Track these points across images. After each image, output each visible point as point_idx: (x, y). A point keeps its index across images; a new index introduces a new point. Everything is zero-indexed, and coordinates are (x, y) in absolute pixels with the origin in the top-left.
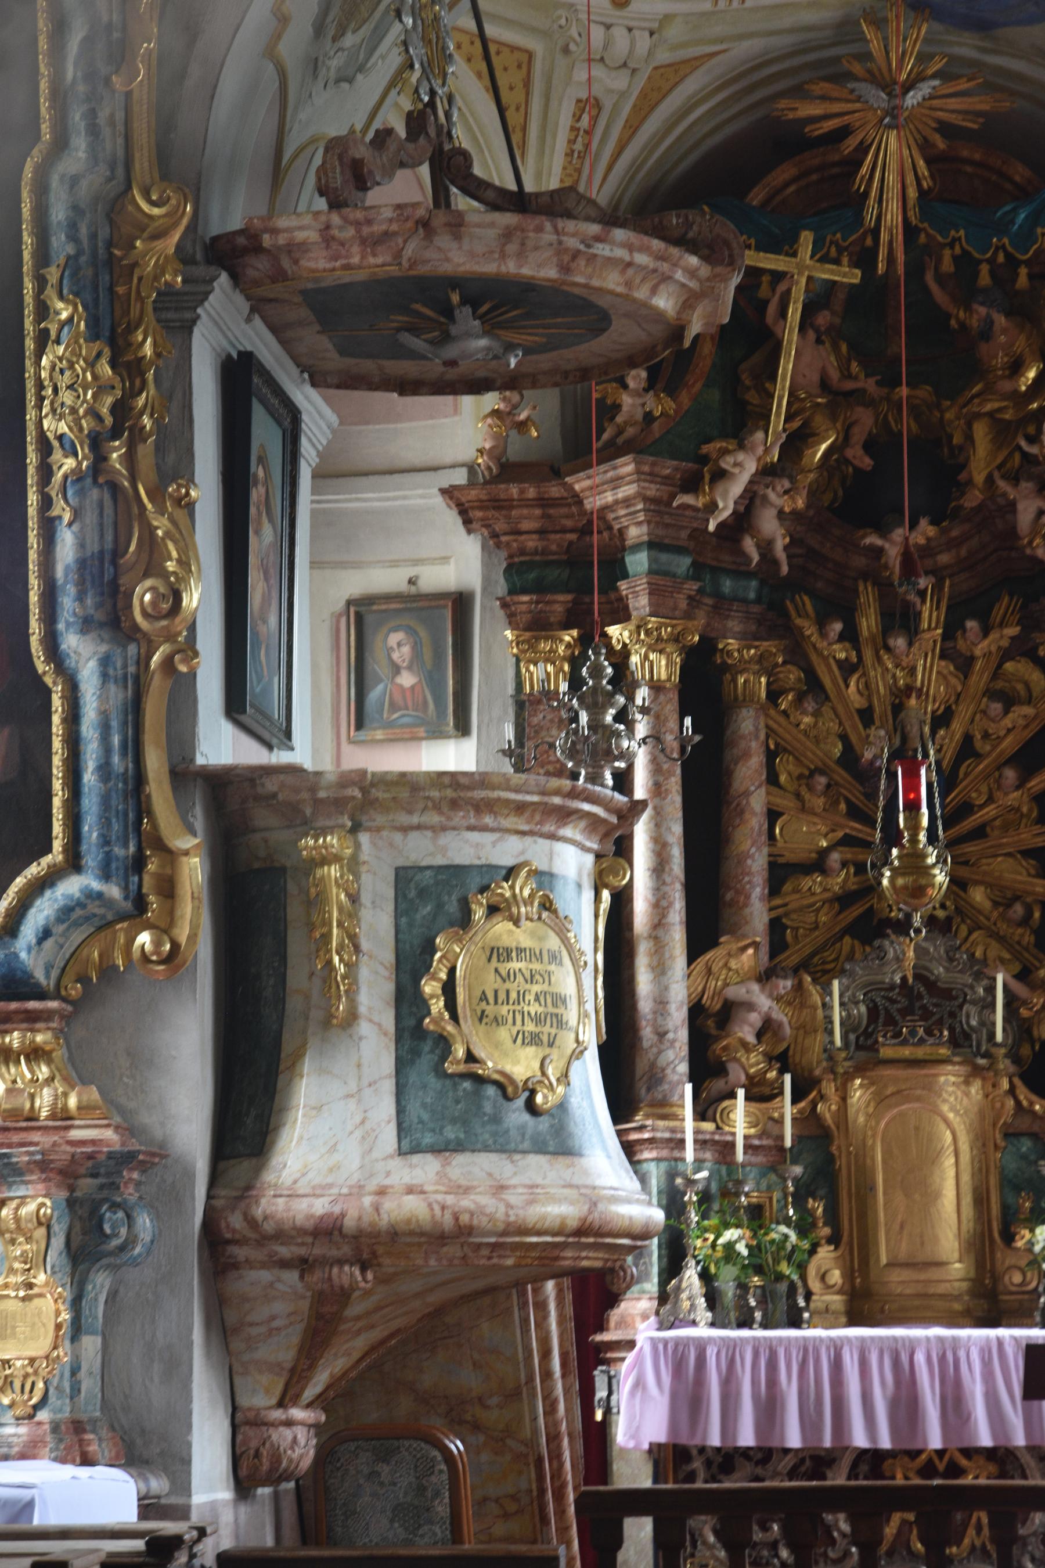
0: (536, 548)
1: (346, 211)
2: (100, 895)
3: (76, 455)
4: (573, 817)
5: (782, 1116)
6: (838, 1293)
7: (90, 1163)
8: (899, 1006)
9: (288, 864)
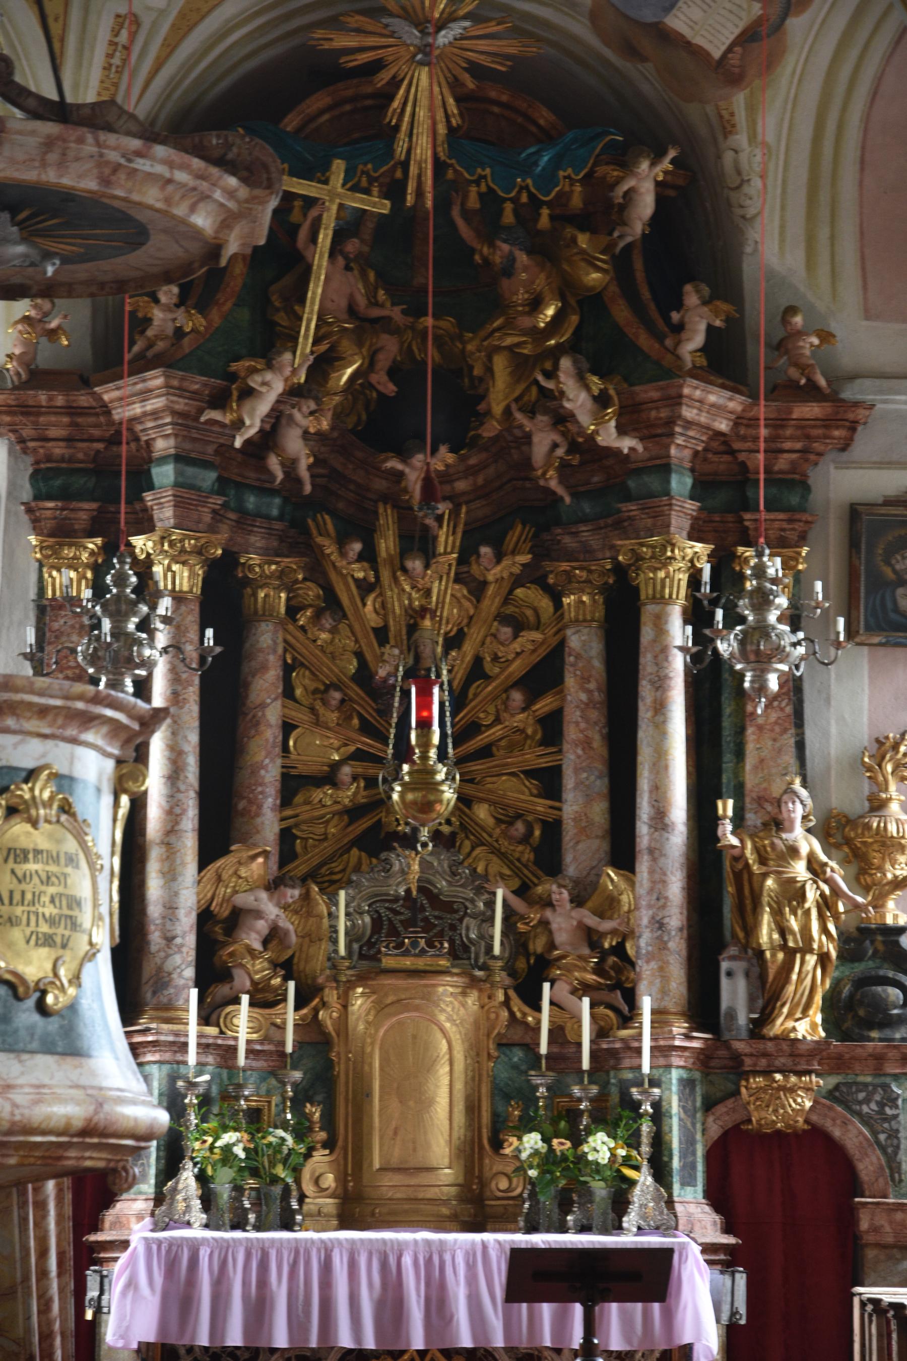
0: (63, 456)
4: (96, 722)
8: (402, 917)
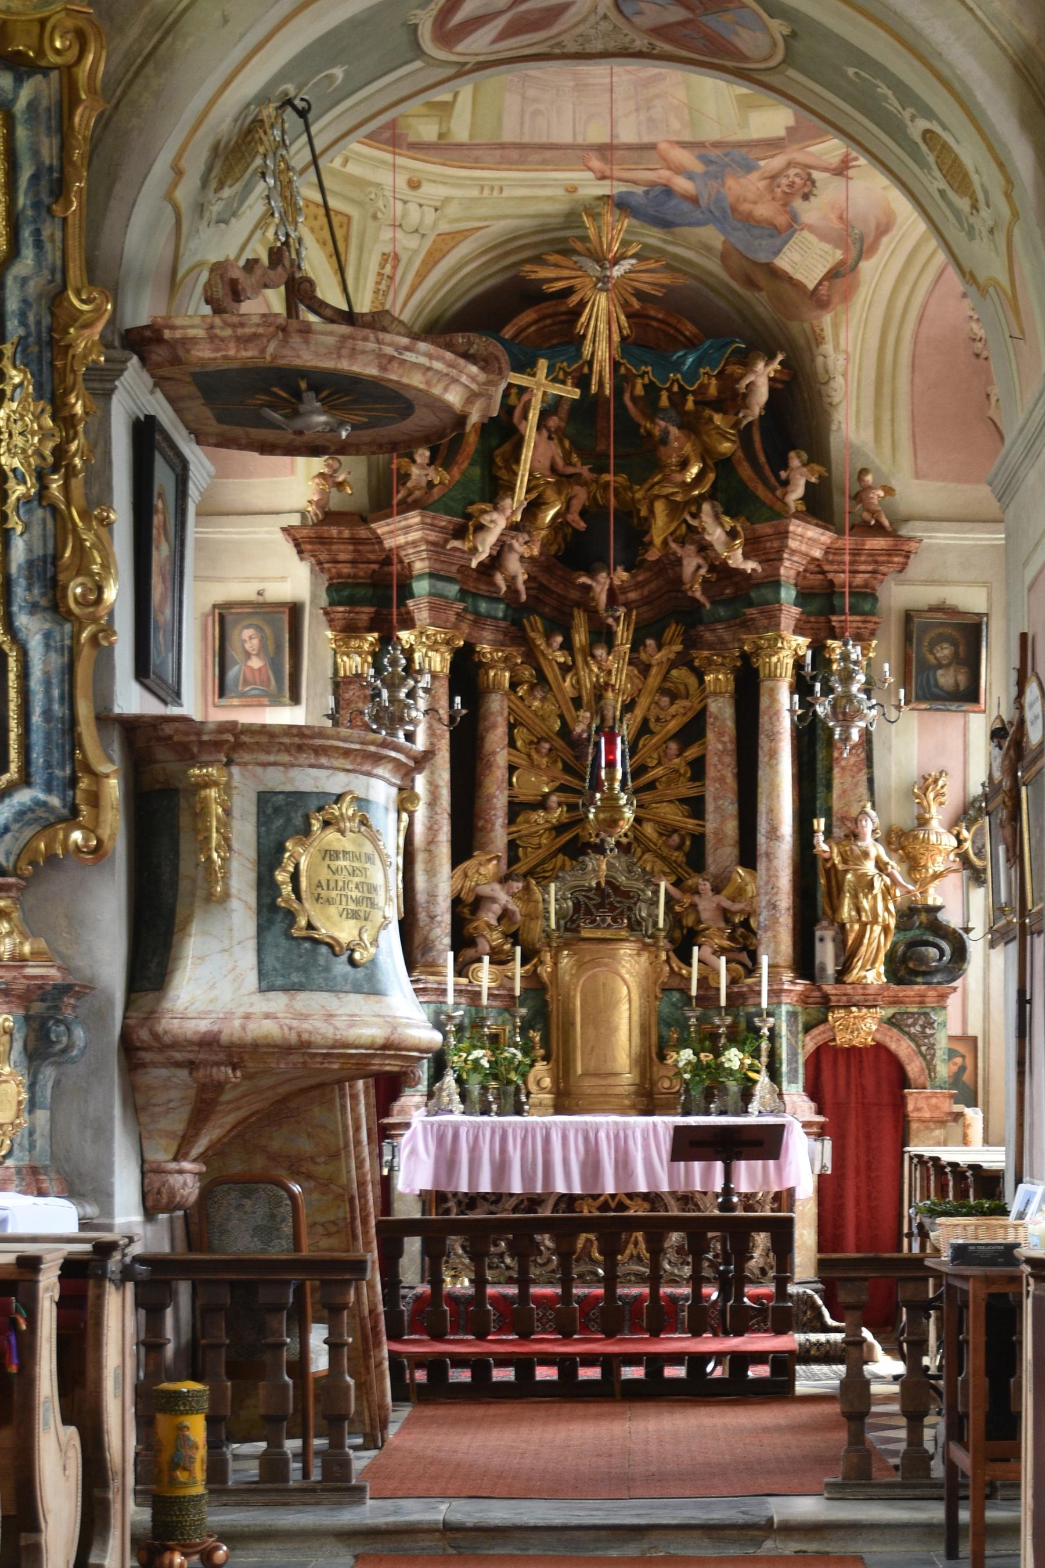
1: (225, 316)
2: (45, 804)
3: (25, 483)
5: (514, 975)
6: (549, 1093)
7: (40, 992)
9: (180, 786)
